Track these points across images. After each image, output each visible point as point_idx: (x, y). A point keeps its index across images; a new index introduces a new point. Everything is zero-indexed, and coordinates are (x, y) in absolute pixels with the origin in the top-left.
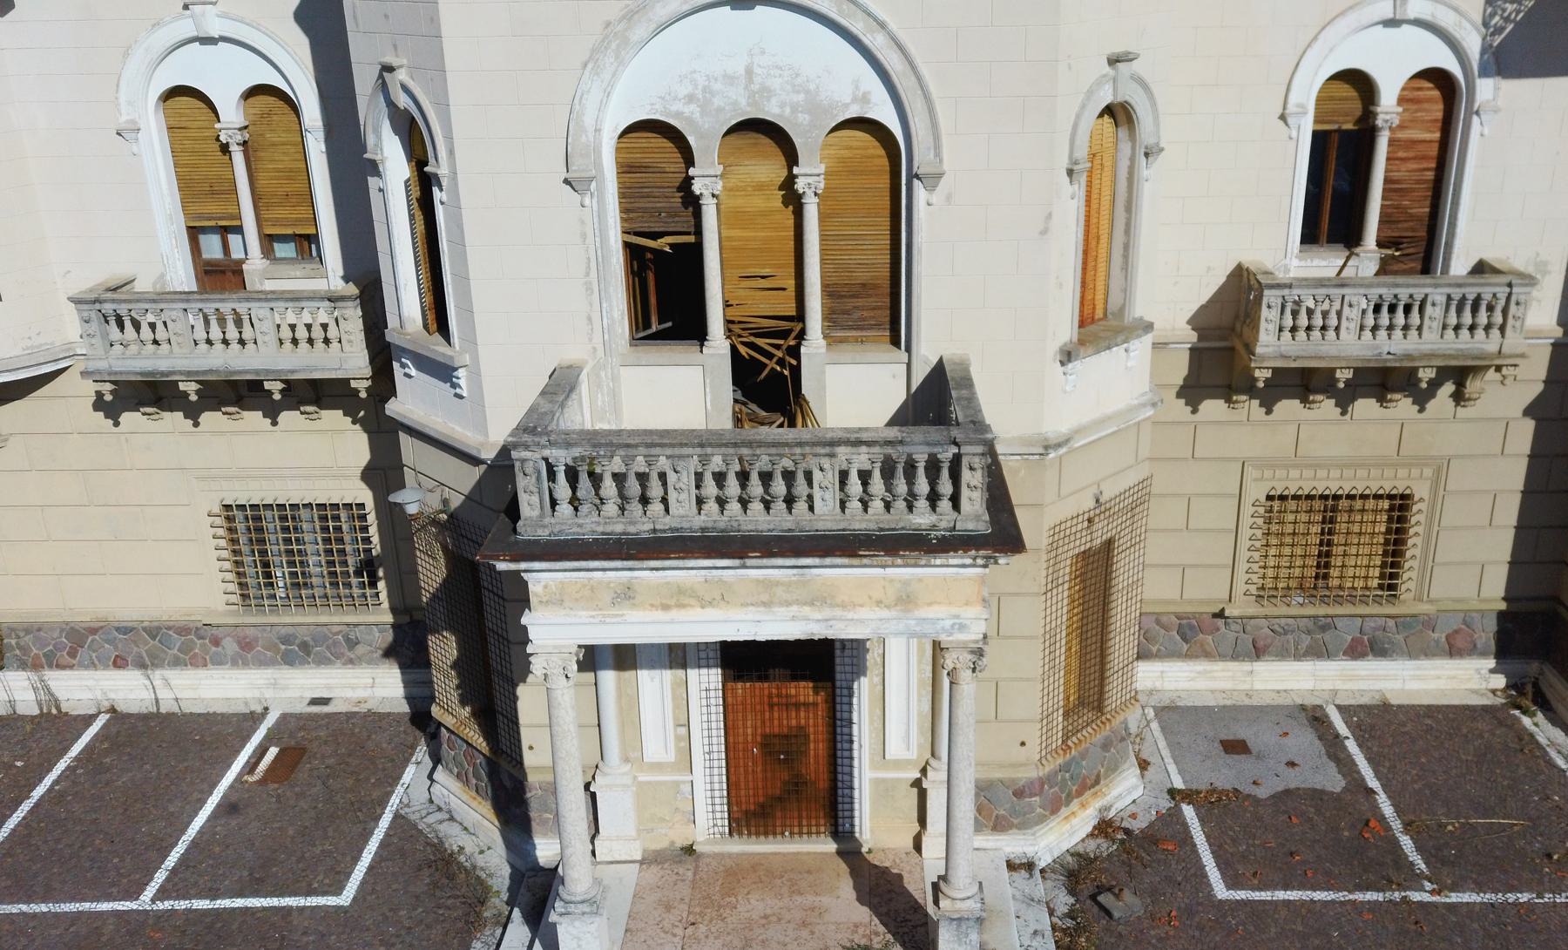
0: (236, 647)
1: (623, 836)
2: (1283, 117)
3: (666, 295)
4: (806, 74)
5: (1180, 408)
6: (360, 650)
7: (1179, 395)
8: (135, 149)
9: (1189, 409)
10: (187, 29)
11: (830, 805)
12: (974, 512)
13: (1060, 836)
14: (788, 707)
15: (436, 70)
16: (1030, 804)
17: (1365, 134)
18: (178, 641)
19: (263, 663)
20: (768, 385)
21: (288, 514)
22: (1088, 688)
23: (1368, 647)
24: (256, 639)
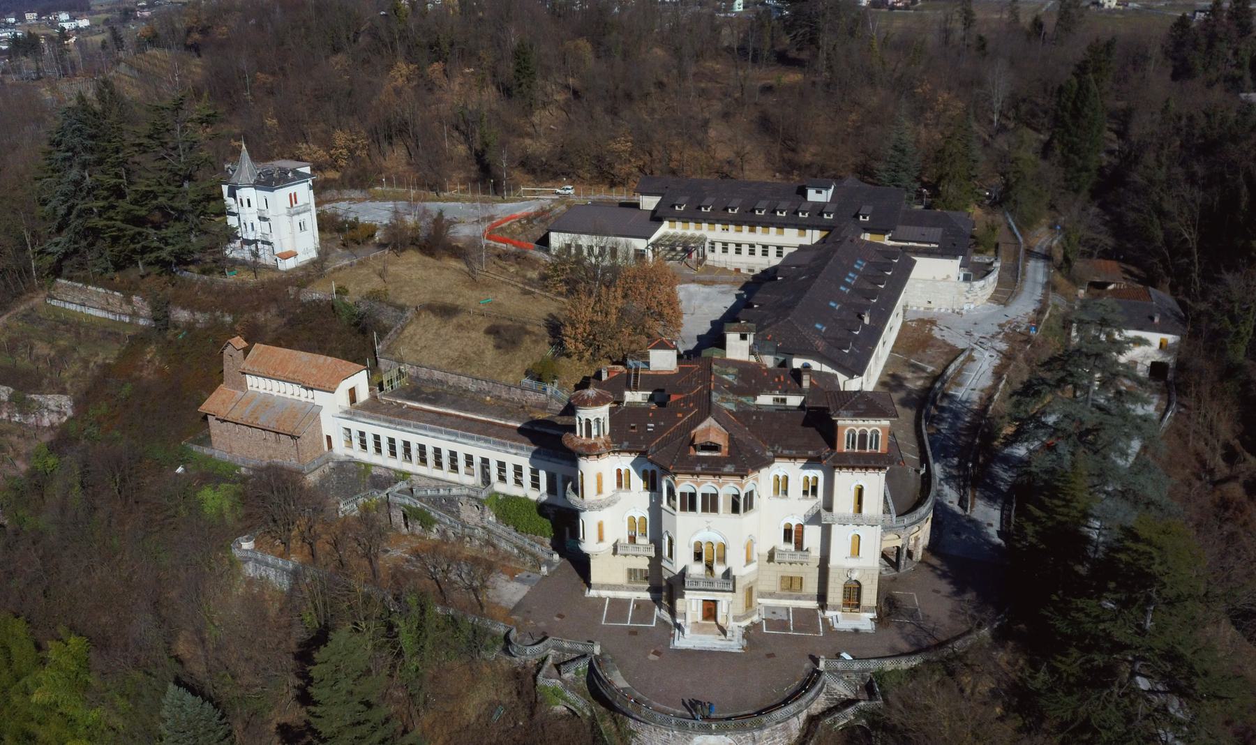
1: (689, 620)
3: (698, 556)
4: (716, 538)
11: (715, 618)
12: (731, 588)
13: (746, 623)
14: (710, 610)
15: (675, 533)
17: (790, 531)
20: (709, 567)
21: (635, 570)
22: (749, 604)
23: (798, 598)
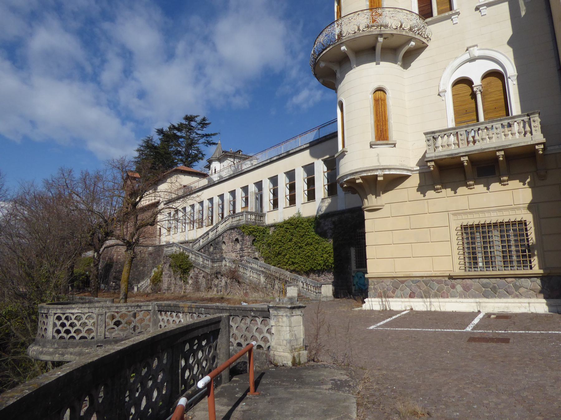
0: (462, 289)
2: (439, 95)
5: (419, 195)
6: (522, 290)
7: (418, 190)
8: (443, 98)
9: (422, 195)
10: (467, 56)
16: (233, 350)
18: (437, 286)
19: (474, 296)
24: (471, 285)
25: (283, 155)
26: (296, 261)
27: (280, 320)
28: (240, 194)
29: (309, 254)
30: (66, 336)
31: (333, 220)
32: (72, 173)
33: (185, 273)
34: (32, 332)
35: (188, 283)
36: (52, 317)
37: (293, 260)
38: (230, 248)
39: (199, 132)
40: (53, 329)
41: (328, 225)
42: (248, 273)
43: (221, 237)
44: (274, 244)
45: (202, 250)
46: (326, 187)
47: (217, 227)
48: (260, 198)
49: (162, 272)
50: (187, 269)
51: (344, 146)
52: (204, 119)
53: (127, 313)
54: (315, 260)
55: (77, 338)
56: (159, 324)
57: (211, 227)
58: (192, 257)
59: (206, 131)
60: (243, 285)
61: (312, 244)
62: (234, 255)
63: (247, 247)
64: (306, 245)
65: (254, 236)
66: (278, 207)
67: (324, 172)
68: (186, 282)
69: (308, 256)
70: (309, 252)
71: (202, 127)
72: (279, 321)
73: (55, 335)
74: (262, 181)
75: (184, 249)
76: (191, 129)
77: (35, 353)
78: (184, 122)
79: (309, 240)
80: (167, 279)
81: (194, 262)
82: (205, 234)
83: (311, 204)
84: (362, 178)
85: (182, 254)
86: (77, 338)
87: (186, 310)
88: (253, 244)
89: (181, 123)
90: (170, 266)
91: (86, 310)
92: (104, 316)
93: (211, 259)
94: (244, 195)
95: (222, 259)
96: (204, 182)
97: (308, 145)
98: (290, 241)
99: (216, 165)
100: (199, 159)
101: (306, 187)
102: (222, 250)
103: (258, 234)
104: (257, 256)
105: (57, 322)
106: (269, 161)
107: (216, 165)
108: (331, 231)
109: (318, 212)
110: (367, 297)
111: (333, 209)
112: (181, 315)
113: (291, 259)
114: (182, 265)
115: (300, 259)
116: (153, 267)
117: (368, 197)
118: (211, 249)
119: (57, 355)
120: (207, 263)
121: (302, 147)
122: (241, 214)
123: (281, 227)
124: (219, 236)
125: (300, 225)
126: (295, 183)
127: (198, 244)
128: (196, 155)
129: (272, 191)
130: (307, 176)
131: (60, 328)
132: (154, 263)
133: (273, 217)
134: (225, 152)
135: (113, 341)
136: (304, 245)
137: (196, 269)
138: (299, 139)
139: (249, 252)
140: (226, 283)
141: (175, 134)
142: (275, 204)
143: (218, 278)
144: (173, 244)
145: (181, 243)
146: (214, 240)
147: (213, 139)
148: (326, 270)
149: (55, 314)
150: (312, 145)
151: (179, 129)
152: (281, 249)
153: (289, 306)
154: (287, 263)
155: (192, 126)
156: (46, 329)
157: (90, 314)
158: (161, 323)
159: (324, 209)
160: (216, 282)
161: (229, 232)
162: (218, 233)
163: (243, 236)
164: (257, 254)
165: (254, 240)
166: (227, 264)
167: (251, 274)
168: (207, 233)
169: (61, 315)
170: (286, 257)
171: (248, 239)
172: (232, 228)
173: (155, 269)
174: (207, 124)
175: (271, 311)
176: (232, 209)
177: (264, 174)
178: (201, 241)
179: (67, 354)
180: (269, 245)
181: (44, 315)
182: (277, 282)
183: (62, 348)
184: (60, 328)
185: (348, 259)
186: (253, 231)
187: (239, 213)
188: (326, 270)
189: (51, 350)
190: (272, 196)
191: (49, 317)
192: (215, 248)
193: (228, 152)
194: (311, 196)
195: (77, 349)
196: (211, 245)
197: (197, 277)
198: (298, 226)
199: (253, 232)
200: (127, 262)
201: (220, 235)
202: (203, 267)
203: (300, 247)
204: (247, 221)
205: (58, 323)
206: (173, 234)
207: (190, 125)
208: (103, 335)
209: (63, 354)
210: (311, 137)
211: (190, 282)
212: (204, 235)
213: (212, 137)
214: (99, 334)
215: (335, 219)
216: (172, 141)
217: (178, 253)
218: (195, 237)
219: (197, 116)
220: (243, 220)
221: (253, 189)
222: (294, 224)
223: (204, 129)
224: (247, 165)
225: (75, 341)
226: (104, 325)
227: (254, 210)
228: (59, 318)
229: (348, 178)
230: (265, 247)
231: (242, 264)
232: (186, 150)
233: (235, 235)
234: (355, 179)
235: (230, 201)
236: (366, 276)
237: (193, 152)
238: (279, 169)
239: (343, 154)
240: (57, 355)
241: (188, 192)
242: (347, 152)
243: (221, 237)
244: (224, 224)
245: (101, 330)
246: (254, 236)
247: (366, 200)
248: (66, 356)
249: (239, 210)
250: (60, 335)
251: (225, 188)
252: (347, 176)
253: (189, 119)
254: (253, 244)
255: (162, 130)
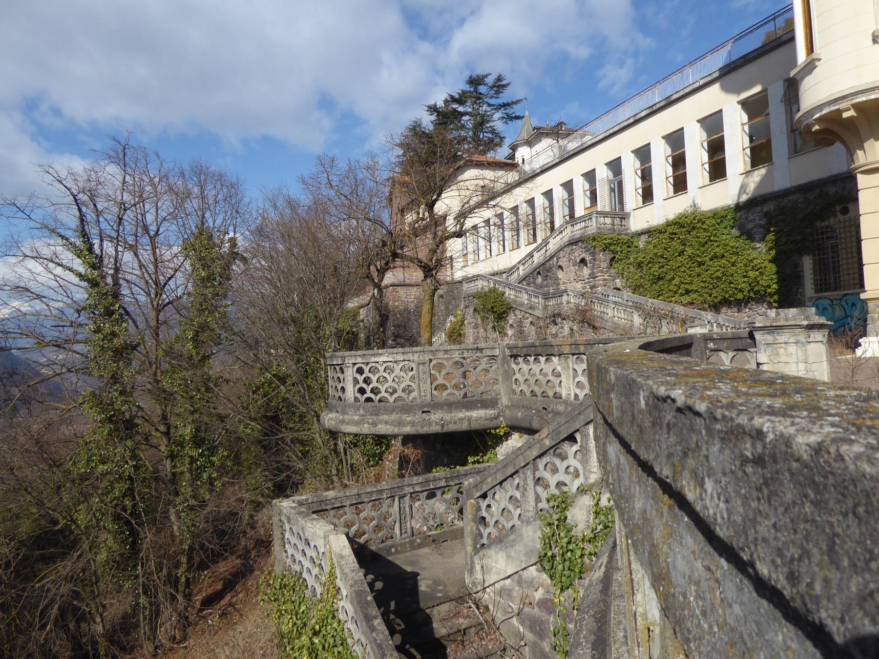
25: (658, 106)
26: (693, 287)
27: (782, 351)
28: (580, 187)
29: (719, 274)
30: (369, 398)
31: (765, 209)
32: (336, 162)
33: (501, 319)
34: (320, 394)
35: (506, 335)
36: (350, 370)
37: (687, 286)
38: (572, 276)
39: (492, 101)
40: (354, 386)
41: (756, 218)
42: (610, 312)
43: (555, 259)
44: (650, 262)
45: (524, 283)
46: (748, 151)
47: (546, 242)
48: (618, 189)
49: (463, 322)
50: (504, 312)
51: (810, 48)
52: (499, 79)
53: (462, 360)
54: (731, 283)
55: (391, 399)
56: (515, 377)
57: (535, 245)
58: (510, 294)
59: (505, 97)
60: (601, 331)
61: (723, 256)
62: (579, 286)
63: (602, 272)
64: (711, 259)
65: (612, 251)
66: (652, 199)
67: (743, 124)
68: (503, 334)
69: (718, 278)
70: (718, 270)
71: (497, 93)
72: (777, 354)
73: (359, 395)
74: (620, 158)
75: (495, 282)
76: (479, 98)
77: (333, 423)
78: (467, 88)
79: (717, 249)
80: (471, 331)
81: (515, 301)
82: (526, 256)
83: (719, 185)
84: (856, 107)
85: (494, 290)
86: (391, 399)
87: (566, 350)
88: (611, 265)
89: (463, 91)
90: (475, 310)
91: (400, 357)
92: (427, 364)
93: (543, 295)
94: (587, 186)
95: (560, 294)
96: (512, 177)
97: (716, 75)
98: (679, 255)
99: (523, 153)
100: (496, 145)
101: (705, 157)
102: (558, 279)
103: (619, 248)
104: (619, 285)
105: (358, 376)
106: (631, 120)
107: (523, 153)
108: (761, 230)
109: (739, 196)
110: (864, 334)
111: (767, 190)
112: (555, 359)
113: (682, 286)
114: (495, 308)
115: (702, 284)
116: (447, 315)
117: (866, 145)
118: (539, 280)
119: (366, 425)
120: (537, 301)
121: (697, 85)
122: (583, 219)
123: (660, 232)
124: (551, 257)
125: (699, 225)
126: (684, 153)
127: (516, 274)
128: (491, 141)
129: (639, 172)
130: (708, 137)
131: (364, 386)
132: (447, 309)
133: (642, 218)
134: (538, 129)
135: (446, 404)
136: (707, 259)
137: (517, 312)
138: (689, 71)
139: (606, 280)
140: (572, 329)
141: (455, 110)
142: (647, 195)
143: (556, 324)
144: (476, 278)
145: (493, 275)
146: (543, 264)
147: (516, 110)
148: (753, 299)
149: (355, 364)
150: (727, 70)
151: (460, 101)
152: (664, 270)
153: (805, 323)
154: (676, 292)
155: (481, 94)
156: (343, 389)
157: (406, 362)
158: (518, 376)
159: (752, 187)
160: (554, 329)
161: (568, 250)
162: (548, 253)
163: (593, 254)
164: (618, 282)
165: (613, 259)
166: (570, 301)
167: (616, 314)
168: (531, 255)
169: (363, 366)
170: (674, 282)
171: (603, 258)
172: (573, 243)
173: (452, 318)
174: (504, 86)
175: (758, 336)
176: (567, 212)
177: (621, 148)
178: (521, 268)
179: (381, 423)
180: (639, 265)
181: (338, 368)
182: (664, 322)
183: (371, 415)
184: (364, 386)
185: (798, 278)
186: (610, 244)
187: (580, 218)
188: (753, 299)
189: (356, 418)
190: (639, 182)
191: (345, 369)
192: (545, 278)
193: (544, 129)
194: (717, 171)
195: (394, 417)
196: (539, 273)
197: (520, 324)
198: (694, 228)
199: (610, 245)
200: (427, 297)
201: (553, 256)
202: (531, 308)
203: (700, 264)
204: (599, 228)
205: (361, 378)
206: (479, 259)
207: (477, 92)
208: (429, 395)
209: (374, 424)
210: (718, 61)
211: (510, 332)
212: (524, 258)
213: (514, 106)
214: (422, 394)
215: (770, 207)
216: (452, 122)
217: (486, 289)
218: (509, 265)
219: (486, 76)
220: (592, 227)
221: (603, 174)
222: (686, 226)
223: (501, 95)
224: (572, 145)
225: (388, 404)
226: (429, 380)
227: (608, 209)
228: (360, 371)
229: (824, 112)
230: (632, 269)
231: (597, 298)
232: (474, 134)
233: (579, 253)
234: (839, 112)
235: (564, 201)
236: (863, 296)
237: (486, 136)
238: (653, 132)
239: (810, 66)
240: (366, 425)
241: (489, 196)
242: (819, 60)
243: (555, 259)
244: (558, 238)
245: (426, 386)
246: (612, 251)
247: (860, 153)
248: (380, 426)
249: (579, 212)
250: (366, 396)
251: (553, 180)
252: (820, 107)
253: (475, 81)
254: (611, 265)
255: (435, 106)
